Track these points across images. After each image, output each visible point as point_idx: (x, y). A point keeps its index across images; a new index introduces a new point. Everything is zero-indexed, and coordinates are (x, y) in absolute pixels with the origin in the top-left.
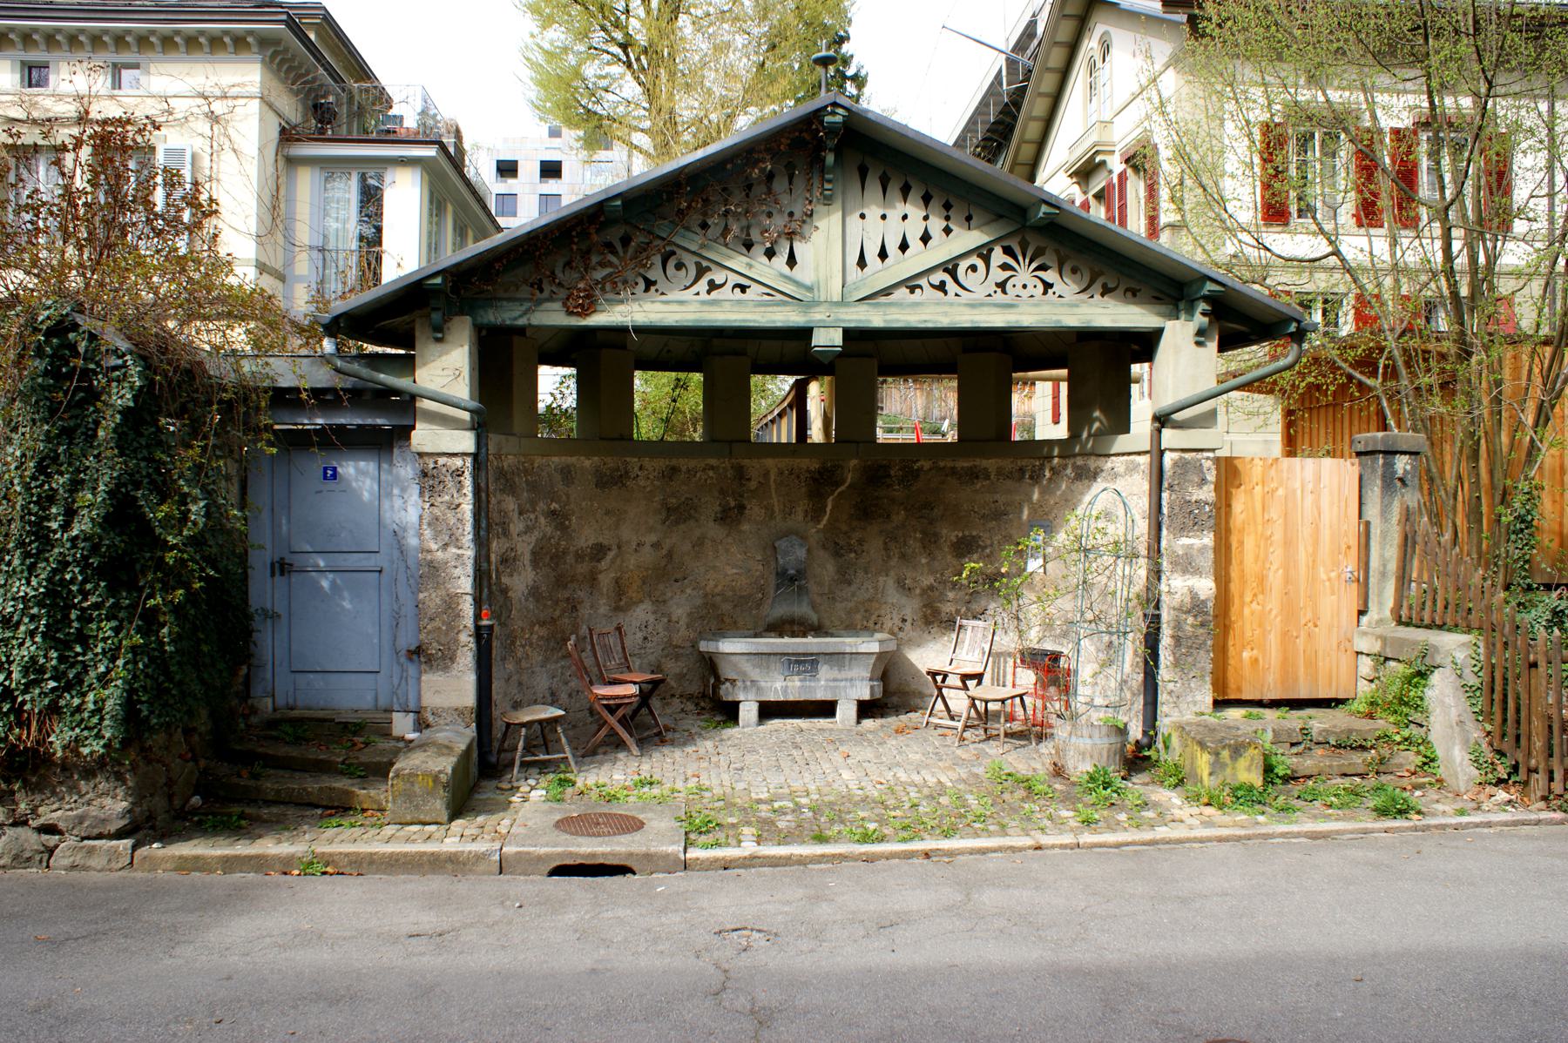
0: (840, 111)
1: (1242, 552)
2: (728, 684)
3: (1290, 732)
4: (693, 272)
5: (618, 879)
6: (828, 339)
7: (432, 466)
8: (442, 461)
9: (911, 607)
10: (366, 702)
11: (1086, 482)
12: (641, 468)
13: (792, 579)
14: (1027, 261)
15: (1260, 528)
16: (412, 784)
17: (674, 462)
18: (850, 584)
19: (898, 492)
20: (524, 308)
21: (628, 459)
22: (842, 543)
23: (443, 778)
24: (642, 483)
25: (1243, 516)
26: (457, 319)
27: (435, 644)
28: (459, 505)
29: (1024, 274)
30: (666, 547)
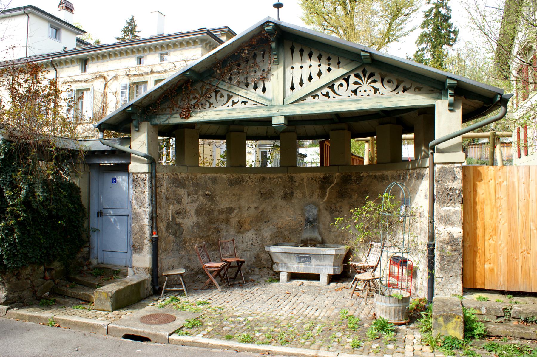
0: (271, 24)
1: (483, 214)
2: (276, 264)
3: (496, 310)
4: (226, 98)
5: (145, 343)
6: (278, 121)
7: (136, 177)
8: (139, 175)
12: (249, 178)
13: (311, 223)
14: (366, 79)
15: (494, 202)
17: (264, 175)
19: (354, 186)
20: (167, 117)
21: (244, 174)
22: (333, 208)
23: (110, 294)
24: (250, 184)
25: (483, 196)
26: (143, 123)
27: (137, 243)
28: (144, 192)
29: (365, 86)
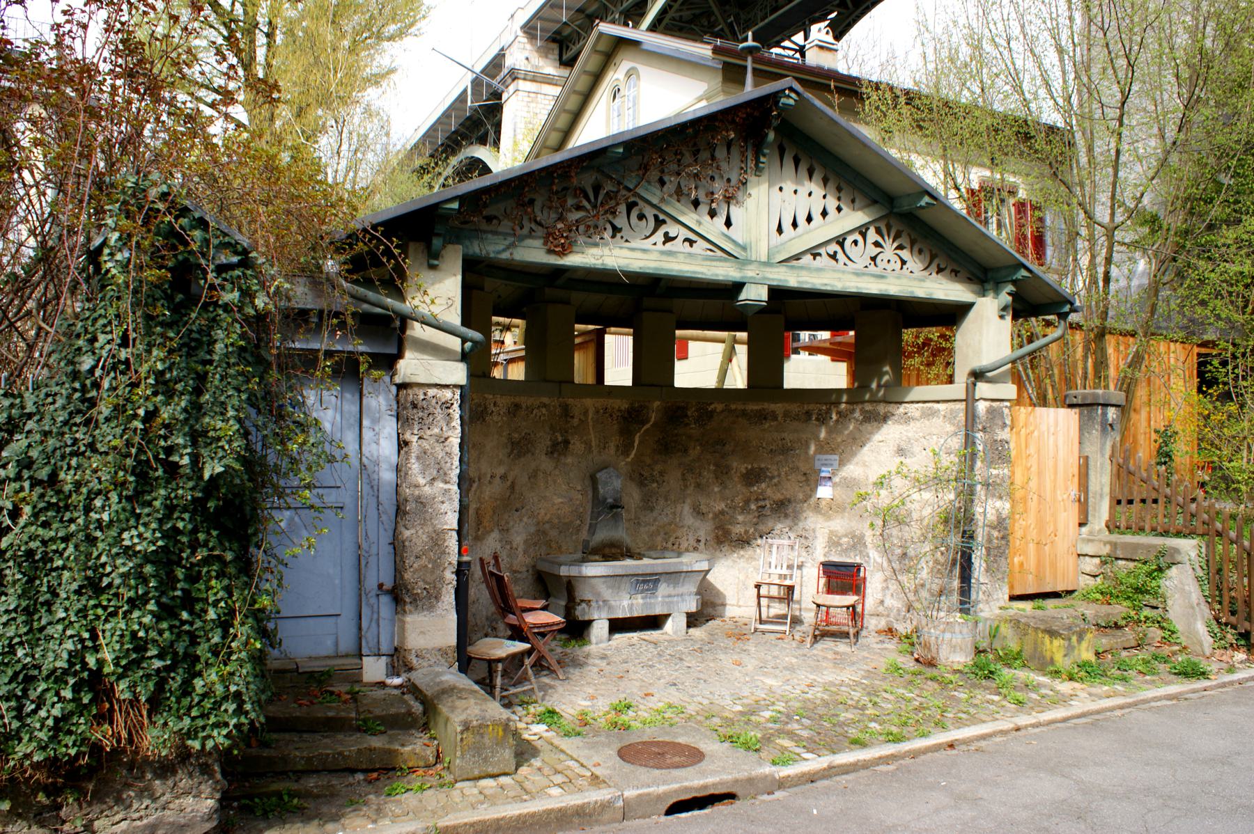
0: (793, 95)
2: (584, 605)
7: (422, 397)
8: (431, 392)
9: (704, 529)
10: (327, 647)
11: (875, 424)
16: (482, 736)
18: (652, 509)
19: (694, 430)
20: (507, 243)
22: (646, 474)
26: (450, 247)
27: (421, 584)
28: (446, 439)
30: (510, 479)
